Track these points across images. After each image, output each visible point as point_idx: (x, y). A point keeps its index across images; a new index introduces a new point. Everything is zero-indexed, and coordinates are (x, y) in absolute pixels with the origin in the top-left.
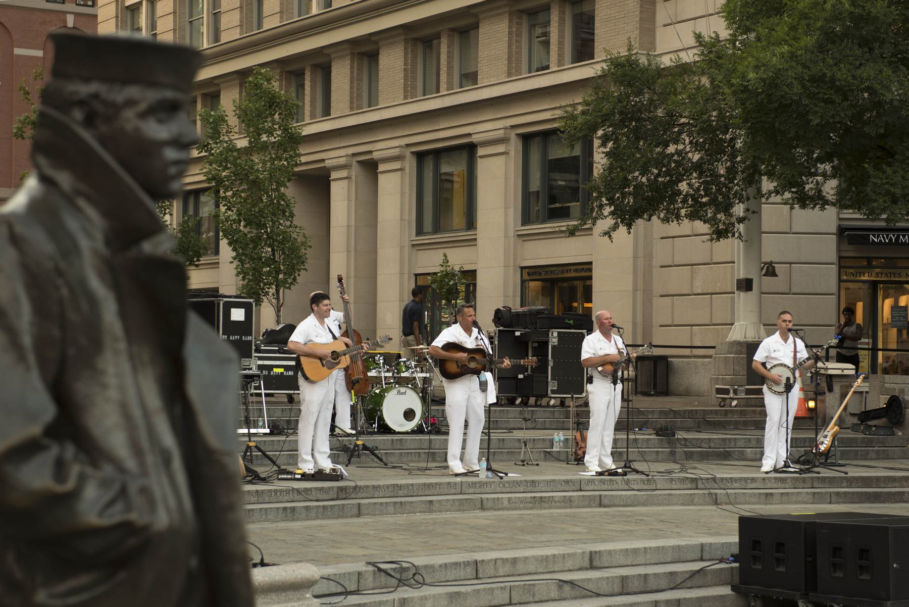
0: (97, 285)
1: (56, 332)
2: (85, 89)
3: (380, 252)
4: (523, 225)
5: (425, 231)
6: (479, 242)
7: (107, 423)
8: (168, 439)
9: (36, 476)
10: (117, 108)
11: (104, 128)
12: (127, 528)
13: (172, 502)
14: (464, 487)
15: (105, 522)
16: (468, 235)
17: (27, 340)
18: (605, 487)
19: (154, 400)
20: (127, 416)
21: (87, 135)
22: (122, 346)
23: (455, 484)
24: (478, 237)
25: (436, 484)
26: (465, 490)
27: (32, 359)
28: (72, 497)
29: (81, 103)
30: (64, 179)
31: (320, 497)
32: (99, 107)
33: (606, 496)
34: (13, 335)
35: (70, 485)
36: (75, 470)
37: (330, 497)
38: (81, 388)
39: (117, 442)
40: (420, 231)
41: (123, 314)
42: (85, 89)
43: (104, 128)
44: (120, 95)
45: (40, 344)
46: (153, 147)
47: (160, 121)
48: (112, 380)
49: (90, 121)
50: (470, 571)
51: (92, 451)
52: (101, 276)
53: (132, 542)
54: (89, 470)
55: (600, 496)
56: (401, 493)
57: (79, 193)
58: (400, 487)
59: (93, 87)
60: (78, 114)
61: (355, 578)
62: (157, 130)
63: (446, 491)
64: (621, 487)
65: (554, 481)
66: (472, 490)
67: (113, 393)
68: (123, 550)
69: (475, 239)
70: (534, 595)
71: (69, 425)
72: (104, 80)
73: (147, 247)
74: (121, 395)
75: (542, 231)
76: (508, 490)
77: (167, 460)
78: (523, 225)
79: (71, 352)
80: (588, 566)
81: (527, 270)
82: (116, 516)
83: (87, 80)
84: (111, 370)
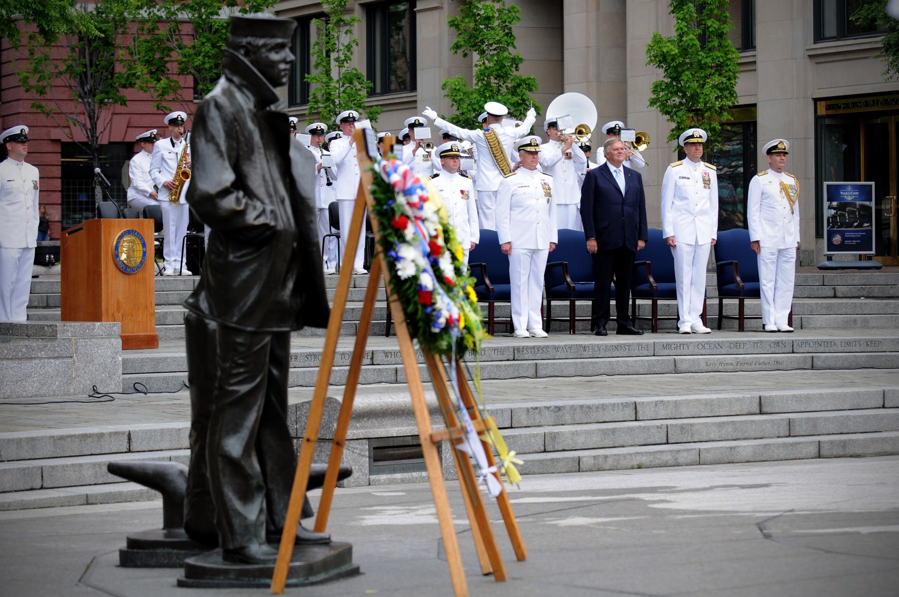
0: (251, 125)
1: (235, 145)
2: (244, 41)
3: (630, 81)
4: (815, 43)
5: (827, 34)
6: (760, 66)
7: (255, 182)
8: (283, 191)
9: (229, 203)
10: (259, 48)
11: (253, 57)
12: (265, 226)
13: (285, 219)
14: (656, 348)
15: (257, 223)
16: (404, 96)
17: (223, 148)
18: (822, 349)
19: (277, 175)
20: (265, 181)
21: (246, 61)
22: (262, 151)
23: (647, 345)
24: (759, 59)
25: (625, 345)
26: (657, 352)
27: (225, 156)
28: (243, 213)
29: (243, 47)
30: (236, 79)
31: (495, 357)
32: (250, 47)
33: (818, 357)
34: (217, 146)
35: (242, 207)
36: (244, 201)
37: (505, 357)
38: (246, 168)
39: (260, 191)
40: (819, 36)
41: (262, 137)
42: (244, 41)
43: (253, 57)
44: (261, 42)
45: (229, 148)
46: (274, 64)
47: (277, 53)
48: (259, 166)
49: (247, 54)
50: (629, 413)
51: (250, 194)
52: (253, 121)
53: (268, 233)
54: (250, 202)
55: (812, 357)
56: (585, 354)
57: (243, 85)
58: (584, 348)
59: (249, 39)
60: (242, 52)
61: (508, 414)
62: (274, 57)
63: (637, 352)
64: (840, 349)
65: (761, 342)
66: (666, 352)
67: (259, 171)
68: (264, 236)
69: (754, 62)
70: (692, 436)
71: (241, 183)
72: (252, 36)
73: (273, 108)
74: (262, 169)
75: (381, 103)
76: (708, 352)
77: (283, 202)
78: (815, 43)
79: (241, 153)
80: (758, 412)
81: (823, 103)
82: (262, 220)
83: (246, 36)
84: (258, 161)
